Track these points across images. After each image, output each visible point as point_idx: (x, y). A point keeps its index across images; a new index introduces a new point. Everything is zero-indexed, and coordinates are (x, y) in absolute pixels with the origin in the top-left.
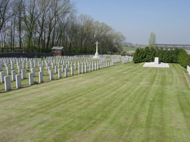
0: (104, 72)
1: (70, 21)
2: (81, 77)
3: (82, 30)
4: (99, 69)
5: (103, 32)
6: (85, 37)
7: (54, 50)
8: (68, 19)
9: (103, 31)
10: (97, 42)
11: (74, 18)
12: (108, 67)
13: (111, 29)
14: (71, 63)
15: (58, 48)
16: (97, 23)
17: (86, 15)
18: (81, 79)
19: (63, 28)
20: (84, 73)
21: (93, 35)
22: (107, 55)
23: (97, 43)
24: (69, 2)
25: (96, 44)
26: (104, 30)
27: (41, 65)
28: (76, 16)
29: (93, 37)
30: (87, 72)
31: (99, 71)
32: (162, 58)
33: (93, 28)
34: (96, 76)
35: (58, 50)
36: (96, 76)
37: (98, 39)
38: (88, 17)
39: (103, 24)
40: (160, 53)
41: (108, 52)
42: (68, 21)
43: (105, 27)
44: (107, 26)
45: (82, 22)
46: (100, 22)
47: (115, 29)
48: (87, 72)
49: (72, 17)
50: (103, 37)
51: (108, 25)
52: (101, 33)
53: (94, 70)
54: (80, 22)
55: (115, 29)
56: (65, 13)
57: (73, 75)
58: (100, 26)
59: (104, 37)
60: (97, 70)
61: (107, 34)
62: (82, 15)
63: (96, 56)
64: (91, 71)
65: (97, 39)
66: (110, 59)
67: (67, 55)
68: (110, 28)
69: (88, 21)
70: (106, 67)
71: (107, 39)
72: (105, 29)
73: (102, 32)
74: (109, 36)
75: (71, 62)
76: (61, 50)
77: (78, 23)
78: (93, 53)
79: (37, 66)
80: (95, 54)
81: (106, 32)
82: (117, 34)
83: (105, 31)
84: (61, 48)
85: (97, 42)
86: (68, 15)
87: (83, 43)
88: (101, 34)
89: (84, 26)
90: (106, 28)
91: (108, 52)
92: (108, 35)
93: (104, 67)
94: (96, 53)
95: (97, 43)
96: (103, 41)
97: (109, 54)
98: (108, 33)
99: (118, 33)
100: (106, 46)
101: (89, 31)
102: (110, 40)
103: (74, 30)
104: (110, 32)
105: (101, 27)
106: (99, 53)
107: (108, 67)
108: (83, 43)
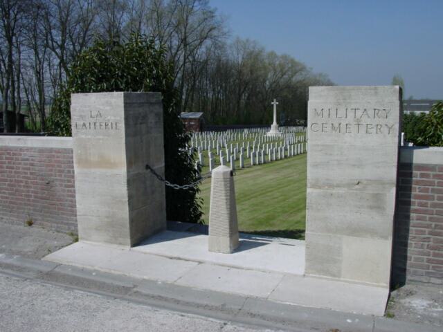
0: (296, 162)
1: (213, 54)
2: (258, 172)
3: (240, 72)
4: (286, 157)
5: (284, 76)
6: (245, 89)
7: (185, 119)
8: (208, 49)
9: (285, 74)
10: (275, 100)
11: (221, 48)
12: (301, 153)
13: (303, 68)
14: (239, 151)
15: (192, 115)
16: (272, 55)
17: (247, 41)
18: (259, 173)
19: (198, 70)
20: (260, 164)
21: (264, 81)
22: (294, 129)
23: (275, 103)
24: (213, 17)
25: (273, 105)
26: (288, 70)
27: (233, 157)
28: (225, 44)
29: (264, 87)
30: (265, 163)
31: (286, 160)
32: (413, 133)
33: (265, 68)
34: (283, 168)
35: (191, 119)
36: (283, 168)
37: (275, 92)
38: (252, 45)
39: (284, 57)
40: (408, 123)
41: (297, 120)
42: (208, 55)
43: (290, 65)
44: (294, 63)
45: (240, 55)
46: (279, 54)
47: (312, 69)
48: (265, 163)
49: (217, 46)
50: (286, 87)
51: (297, 60)
52: (281, 78)
53: (276, 160)
54: (235, 56)
55: (312, 69)
56: (202, 39)
57: (243, 167)
58: (277, 63)
59: (288, 87)
60: (281, 159)
61: (294, 79)
62: (238, 41)
63: (273, 131)
64: (271, 160)
65: (273, 91)
66: (305, 138)
67: (210, 129)
68: (300, 67)
69: (251, 53)
70: (298, 154)
71: (296, 91)
72: (289, 68)
73: (282, 76)
74: (298, 85)
75: (239, 149)
76: (199, 119)
77: (231, 57)
78: (267, 125)
79: (266, 159)
80: (270, 127)
81: (292, 77)
82: (318, 78)
83: (290, 73)
84: (199, 115)
85: (275, 100)
86: (208, 42)
87: (243, 101)
88: (282, 80)
89: (244, 65)
90: (292, 66)
91: (297, 120)
92: (298, 82)
93: (294, 153)
94: (272, 123)
95: (275, 103)
96: (286, 96)
97: (300, 125)
98: (297, 78)
99: (320, 75)
100: (292, 106)
101: (211, 23)
102: (301, 93)
103: (223, 72)
104: (301, 74)
105: (280, 64)
106: (280, 124)
107: (301, 153)
108: (243, 101)
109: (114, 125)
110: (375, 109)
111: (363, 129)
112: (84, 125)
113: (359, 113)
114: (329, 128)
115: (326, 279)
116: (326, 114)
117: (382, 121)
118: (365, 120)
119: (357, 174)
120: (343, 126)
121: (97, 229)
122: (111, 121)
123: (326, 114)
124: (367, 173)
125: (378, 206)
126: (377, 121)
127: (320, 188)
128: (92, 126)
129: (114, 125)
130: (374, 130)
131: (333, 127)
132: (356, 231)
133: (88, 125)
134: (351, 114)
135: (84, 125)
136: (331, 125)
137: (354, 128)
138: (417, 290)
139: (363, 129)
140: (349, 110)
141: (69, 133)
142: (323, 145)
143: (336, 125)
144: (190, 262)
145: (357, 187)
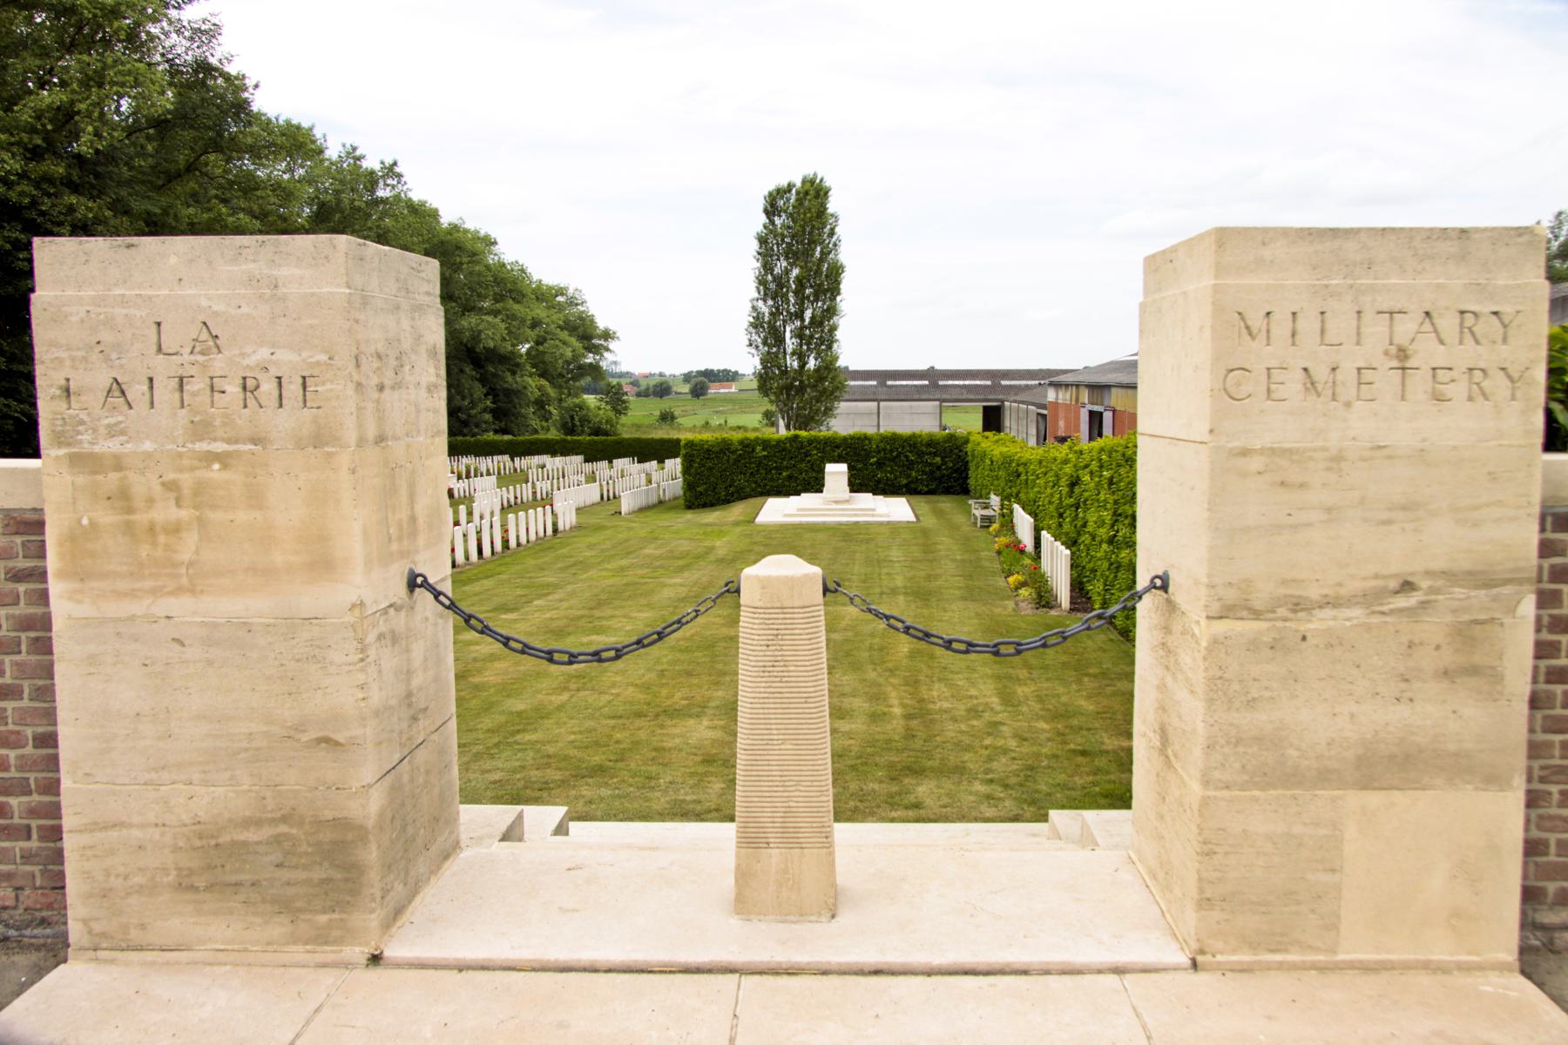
109: (293, 389)
110: (1462, 312)
111: (1419, 383)
112: (118, 388)
113: (1406, 328)
114: (1292, 385)
115: (1280, 966)
116: (1281, 329)
117: (1484, 356)
118: (1427, 353)
119: (1398, 553)
120: (1347, 373)
121: (185, 886)
122: (274, 371)
123: (1281, 329)
124: (1440, 543)
125: (1470, 669)
126: (1466, 355)
127: (1256, 614)
128: (165, 392)
129: (293, 389)
130: (1458, 391)
131: (1310, 383)
132: (1389, 766)
133: (137, 391)
134: (1376, 329)
135: (118, 388)
136: (1300, 374)
137: (1385, 379)
138: (1094, 444)
139: (1419, 383)
140: (1368, 316)
141: (1129, 807)
142: (1273, 451)
143: (1321, 373)
144: (1088, 978)
145: (1402, 602)
